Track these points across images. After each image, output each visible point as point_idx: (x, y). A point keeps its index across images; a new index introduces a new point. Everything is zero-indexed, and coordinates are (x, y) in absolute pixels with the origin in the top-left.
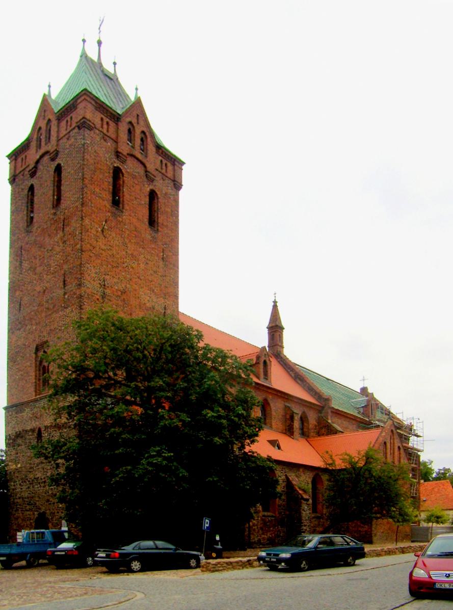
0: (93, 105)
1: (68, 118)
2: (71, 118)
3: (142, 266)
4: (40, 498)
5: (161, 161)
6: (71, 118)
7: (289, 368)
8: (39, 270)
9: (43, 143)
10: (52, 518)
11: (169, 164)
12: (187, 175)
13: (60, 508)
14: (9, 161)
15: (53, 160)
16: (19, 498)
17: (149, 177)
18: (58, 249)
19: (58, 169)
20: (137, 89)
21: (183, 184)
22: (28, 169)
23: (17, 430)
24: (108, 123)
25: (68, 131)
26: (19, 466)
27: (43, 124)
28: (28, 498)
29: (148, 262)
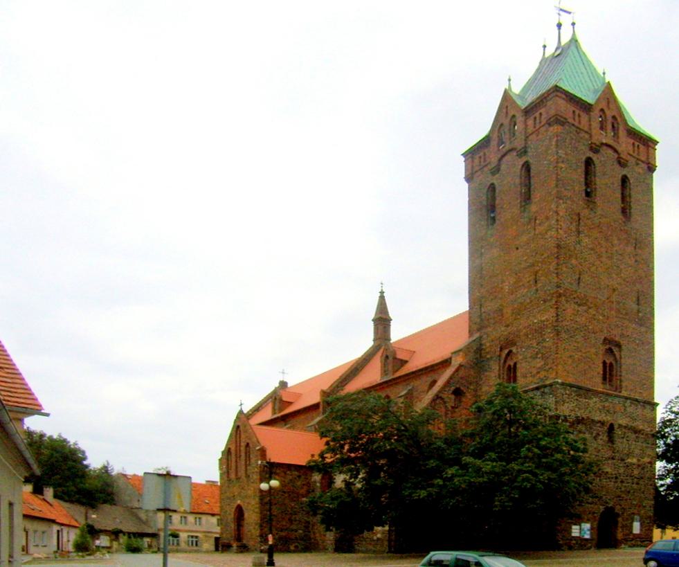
0: (564, 99)
1: (537, 115)
2: (541, 114)
5: (574, 112)
6: (541, 114)
14: (463, 159)
17: (621, 163)
20: (510, 80)
21: (657, 164)
24: (579, 116)
25: (537, 127)
27: (506, 122)
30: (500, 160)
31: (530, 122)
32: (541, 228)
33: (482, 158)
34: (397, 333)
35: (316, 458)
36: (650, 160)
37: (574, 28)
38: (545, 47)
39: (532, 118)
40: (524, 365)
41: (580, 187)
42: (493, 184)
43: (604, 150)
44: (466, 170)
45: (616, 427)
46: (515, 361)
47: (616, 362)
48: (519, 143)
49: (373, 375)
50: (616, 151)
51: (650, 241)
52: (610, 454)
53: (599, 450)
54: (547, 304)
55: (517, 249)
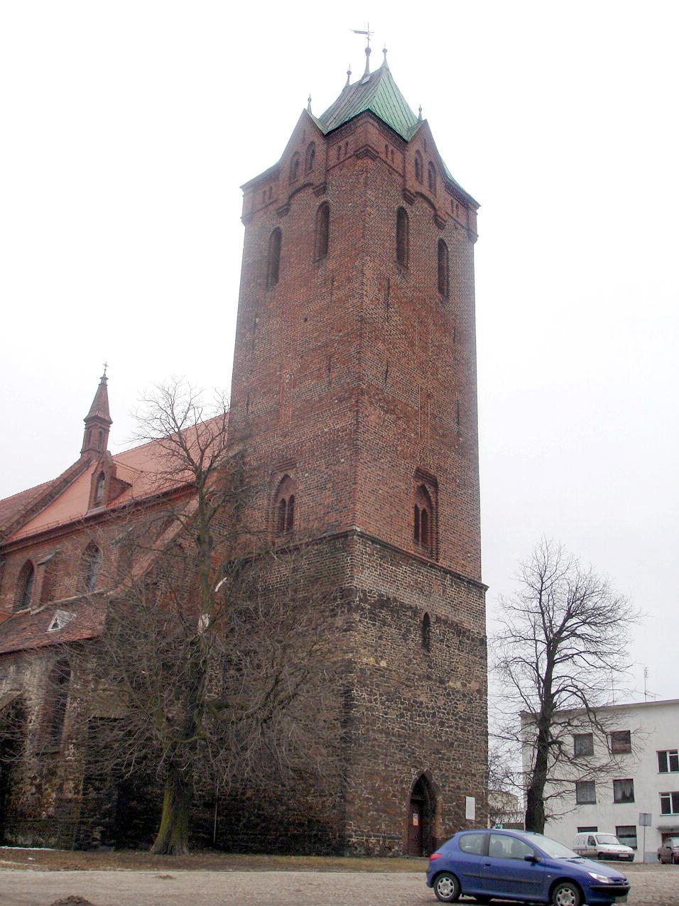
1: (342, 144)
2: (347, 144)
4: (422, 742)
6: (347, 144)
10: (444, 786)
12: (483, 221)
13: (459, 769)
16: (381, 731)
20: (310, 100)
22: (275, 206)
25: (342, 158)
27: (303, 150)
28: (400, 736)
30: (291, 197)
31: (333, 152)
32: (341, 293)
33: (268, 193)
34: (118, 443)
36: (471, 227)
37: (385, 55)
38: (349, 73)
39: (336, 147)
40: (305, 499)
41: (391, 245)
42: (278, 228)
43: (419, 202)
44: (245, 208)
45: (432, 620)
46: (292, 493)
47: (431, 508)
48: (317, 178)
49: (75, 506)
50: (433, 206)
51: (8, 767)
52: (423, 669)
53: (410, 660)
54: (344, 404)
55: (306, 320)
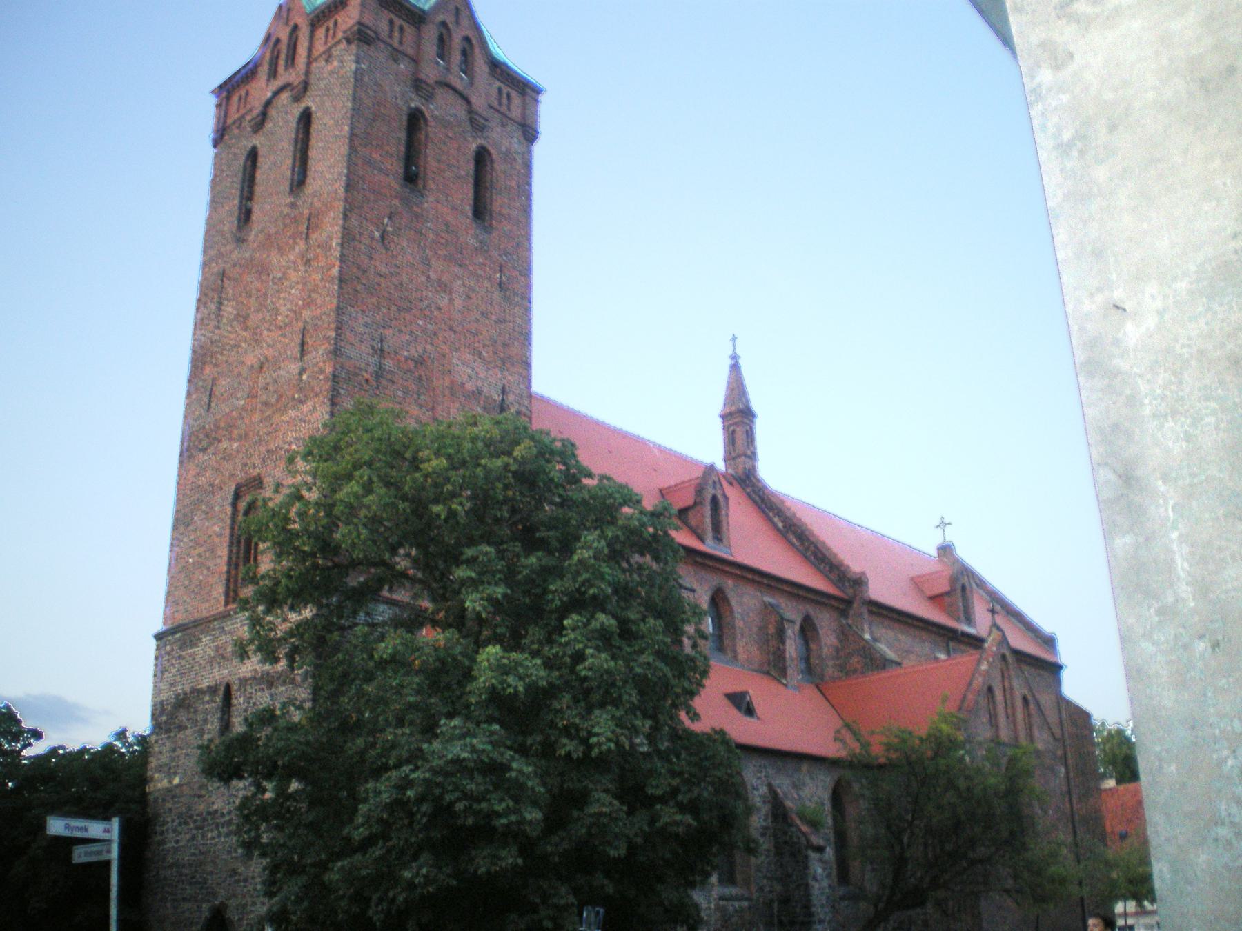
1: (243, 93)
3: (458, 303)
7: (771, 509)
8: (254, 319)
9: (281, 69)
11: (514, 94)
12: (548, 114)
15: (297, 99)
17: (476, 123)
18: (294, 276)
19: (306, 118)
22: (248, 118)
23: (179, 689)
24: (401, 29)
25: (331, 42)
26: (176, 781)
27: (284, 35)
29: (470, 294)
35: (170, 860)
